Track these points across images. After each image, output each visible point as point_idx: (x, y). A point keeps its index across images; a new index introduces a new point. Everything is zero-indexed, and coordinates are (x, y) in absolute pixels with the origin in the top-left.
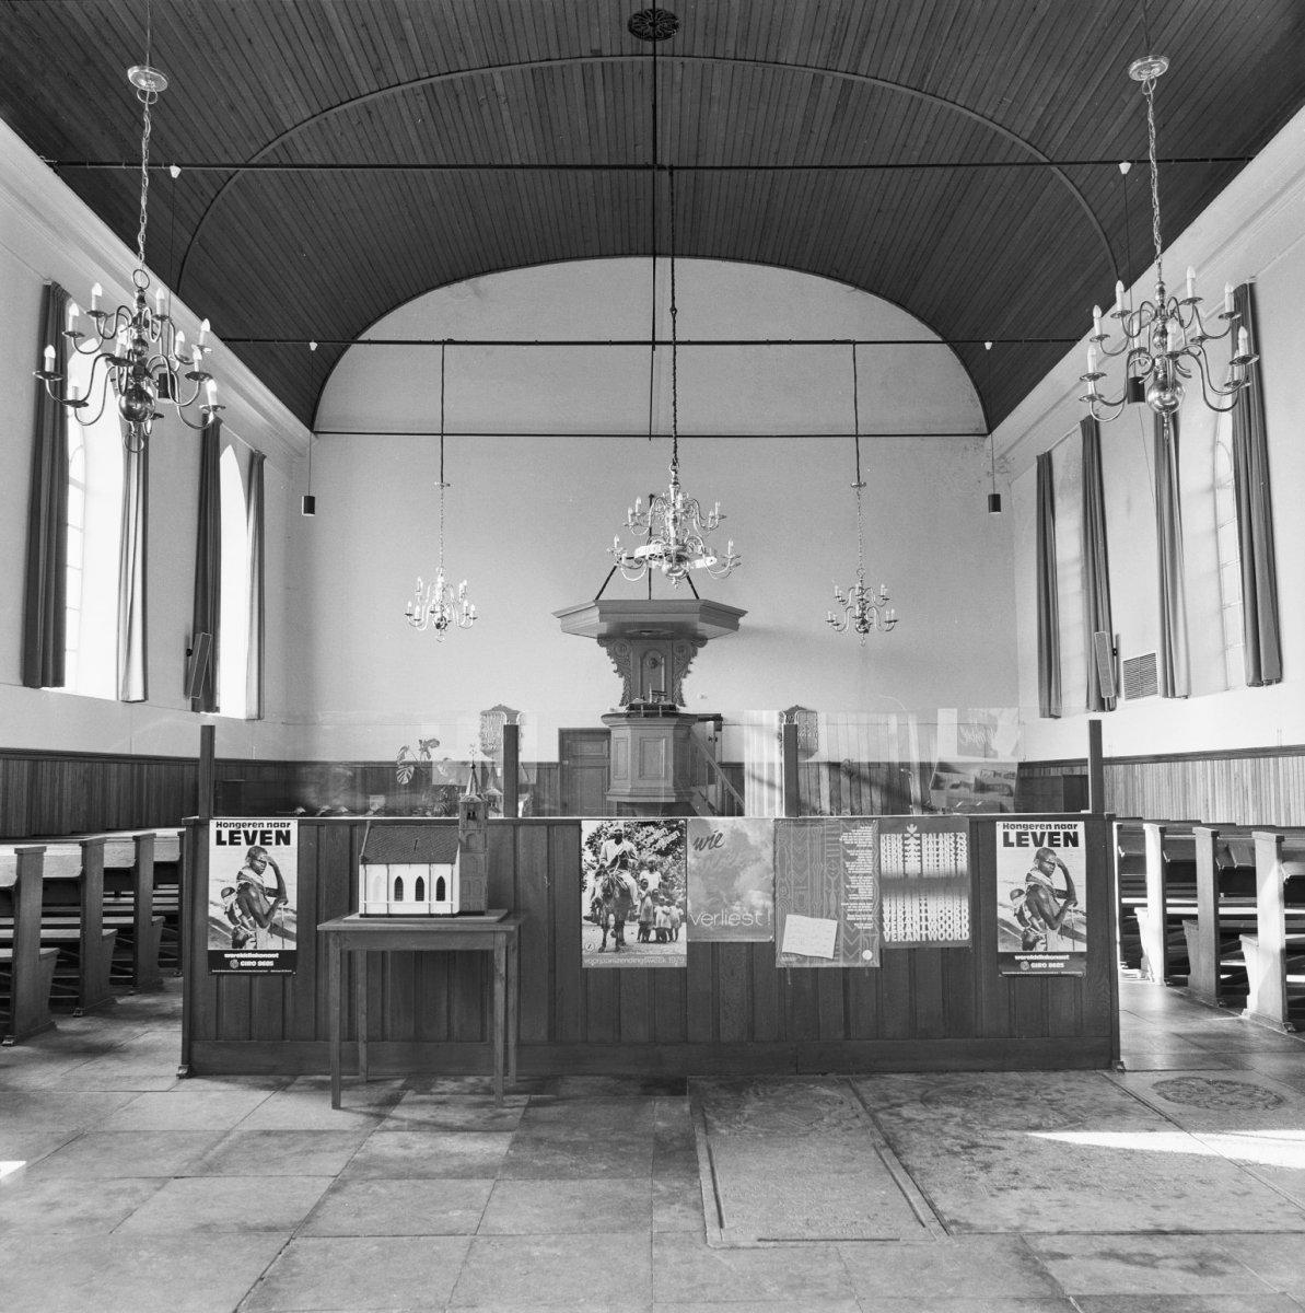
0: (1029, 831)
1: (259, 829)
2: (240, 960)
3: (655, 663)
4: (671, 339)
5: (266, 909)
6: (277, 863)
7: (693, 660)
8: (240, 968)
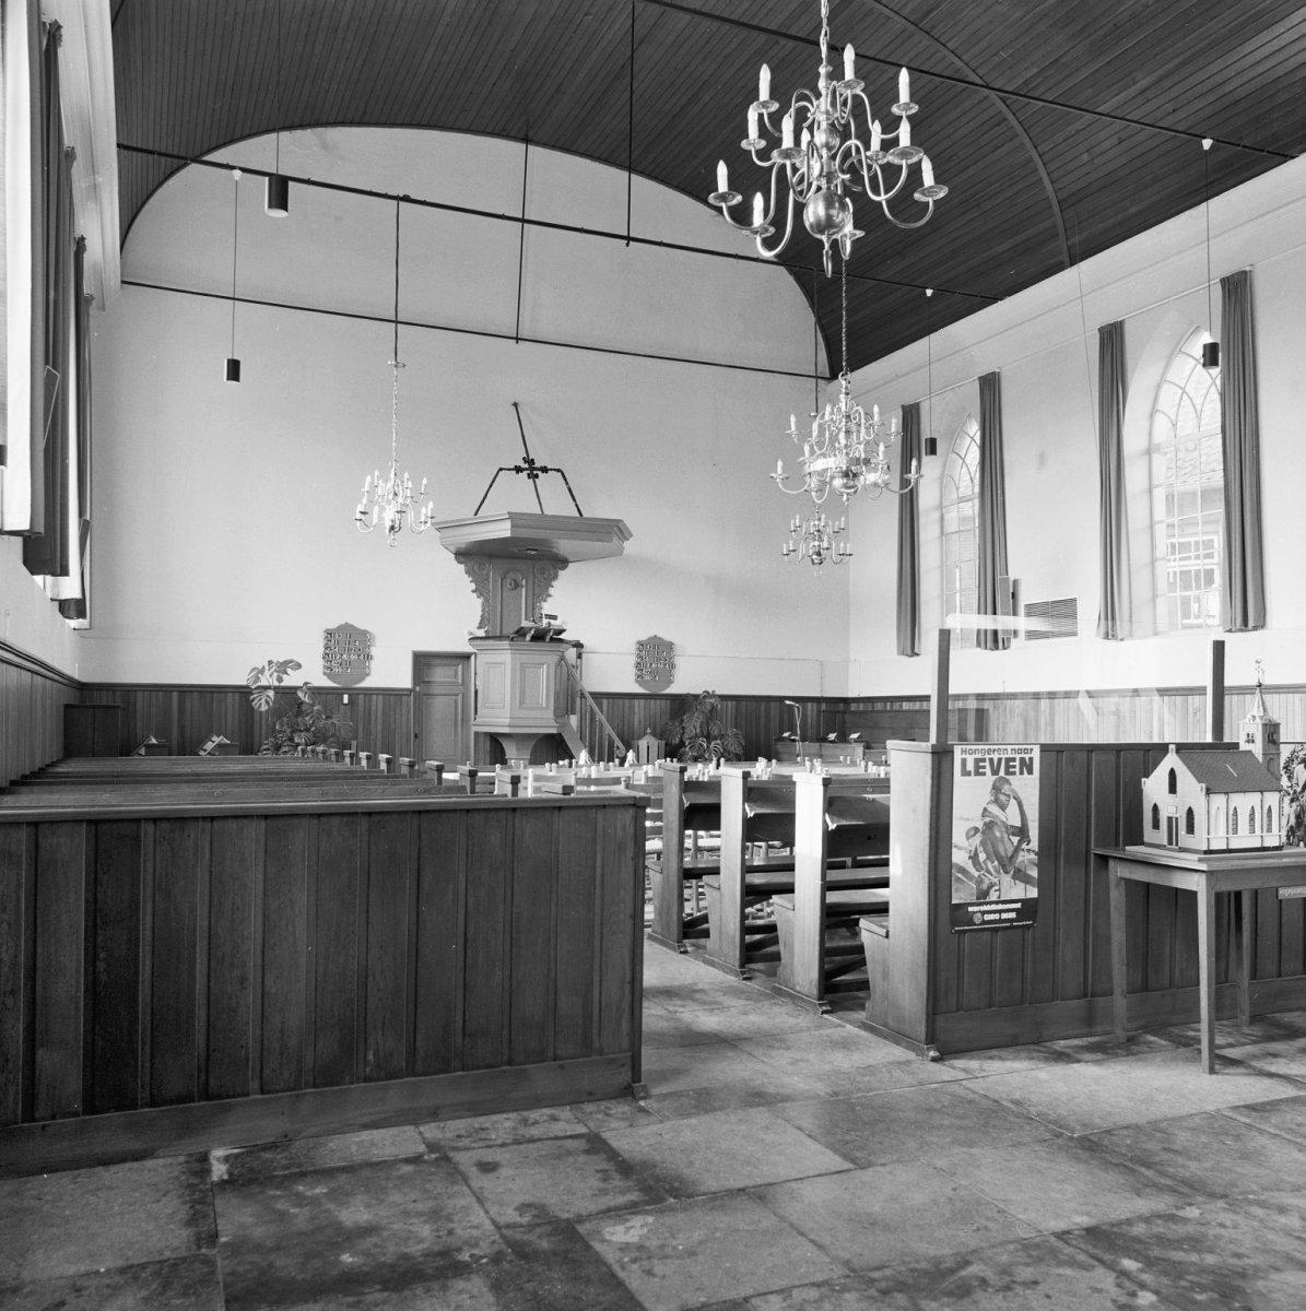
0: (987, 756)
1: (1004, 756)
2: (984, 913)
3: (517, 585)
4: (626, 234)
5: (1010, 851)
6: (1022, 798)
7: (554, 583)
8: (984, 922)
